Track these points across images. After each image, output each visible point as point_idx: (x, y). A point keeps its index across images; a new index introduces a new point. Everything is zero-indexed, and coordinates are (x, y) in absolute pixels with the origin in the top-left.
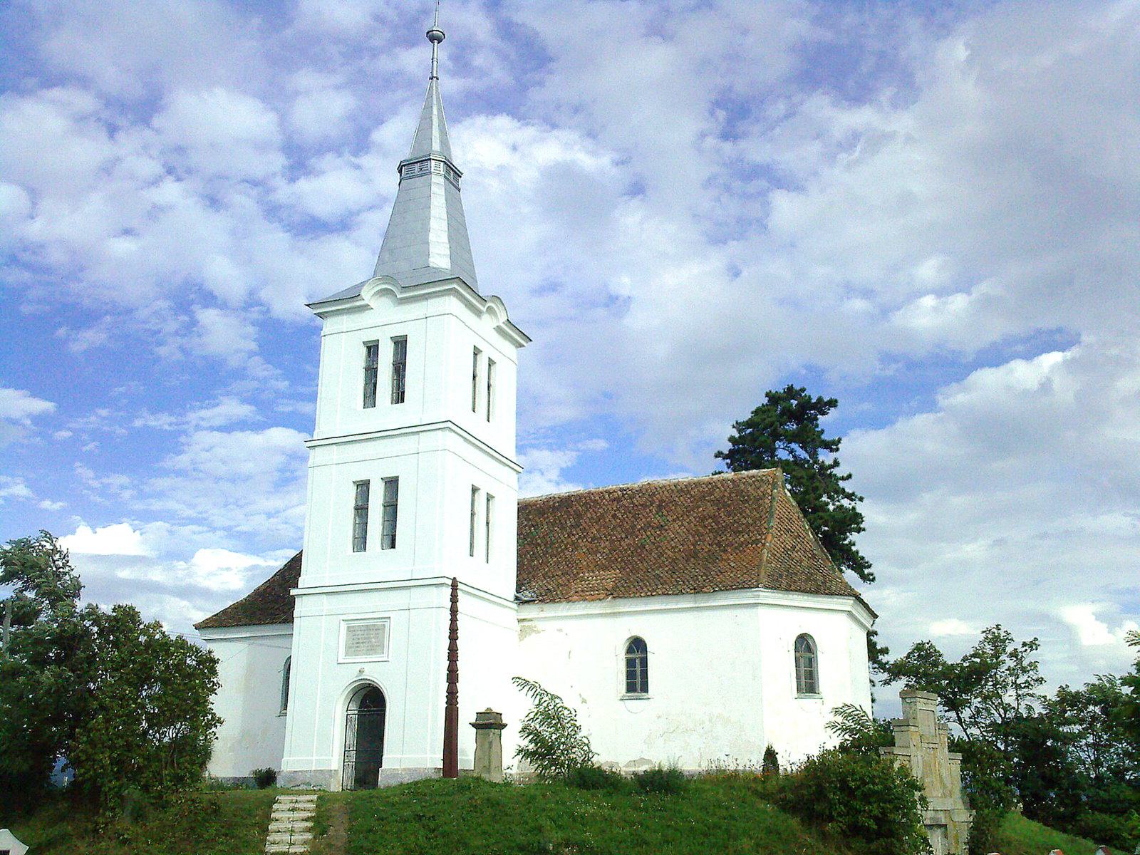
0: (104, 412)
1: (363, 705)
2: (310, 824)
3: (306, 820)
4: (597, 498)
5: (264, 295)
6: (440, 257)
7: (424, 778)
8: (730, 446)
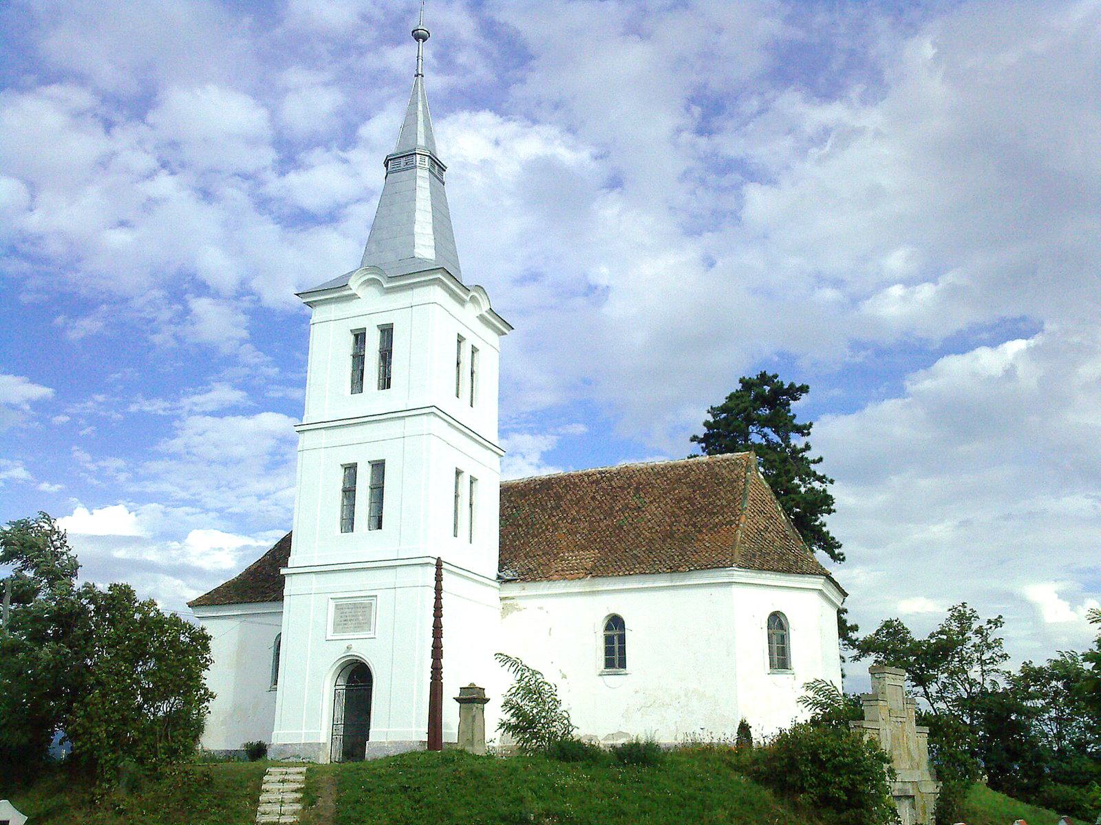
0: (100, 398)
1: (350, 680)
2: (299, 795)
3: (296, 791)
4: (577, 480)
5: (255, 284)
6: (425, 248)
7: (409, 751)
8: (705, 430)
